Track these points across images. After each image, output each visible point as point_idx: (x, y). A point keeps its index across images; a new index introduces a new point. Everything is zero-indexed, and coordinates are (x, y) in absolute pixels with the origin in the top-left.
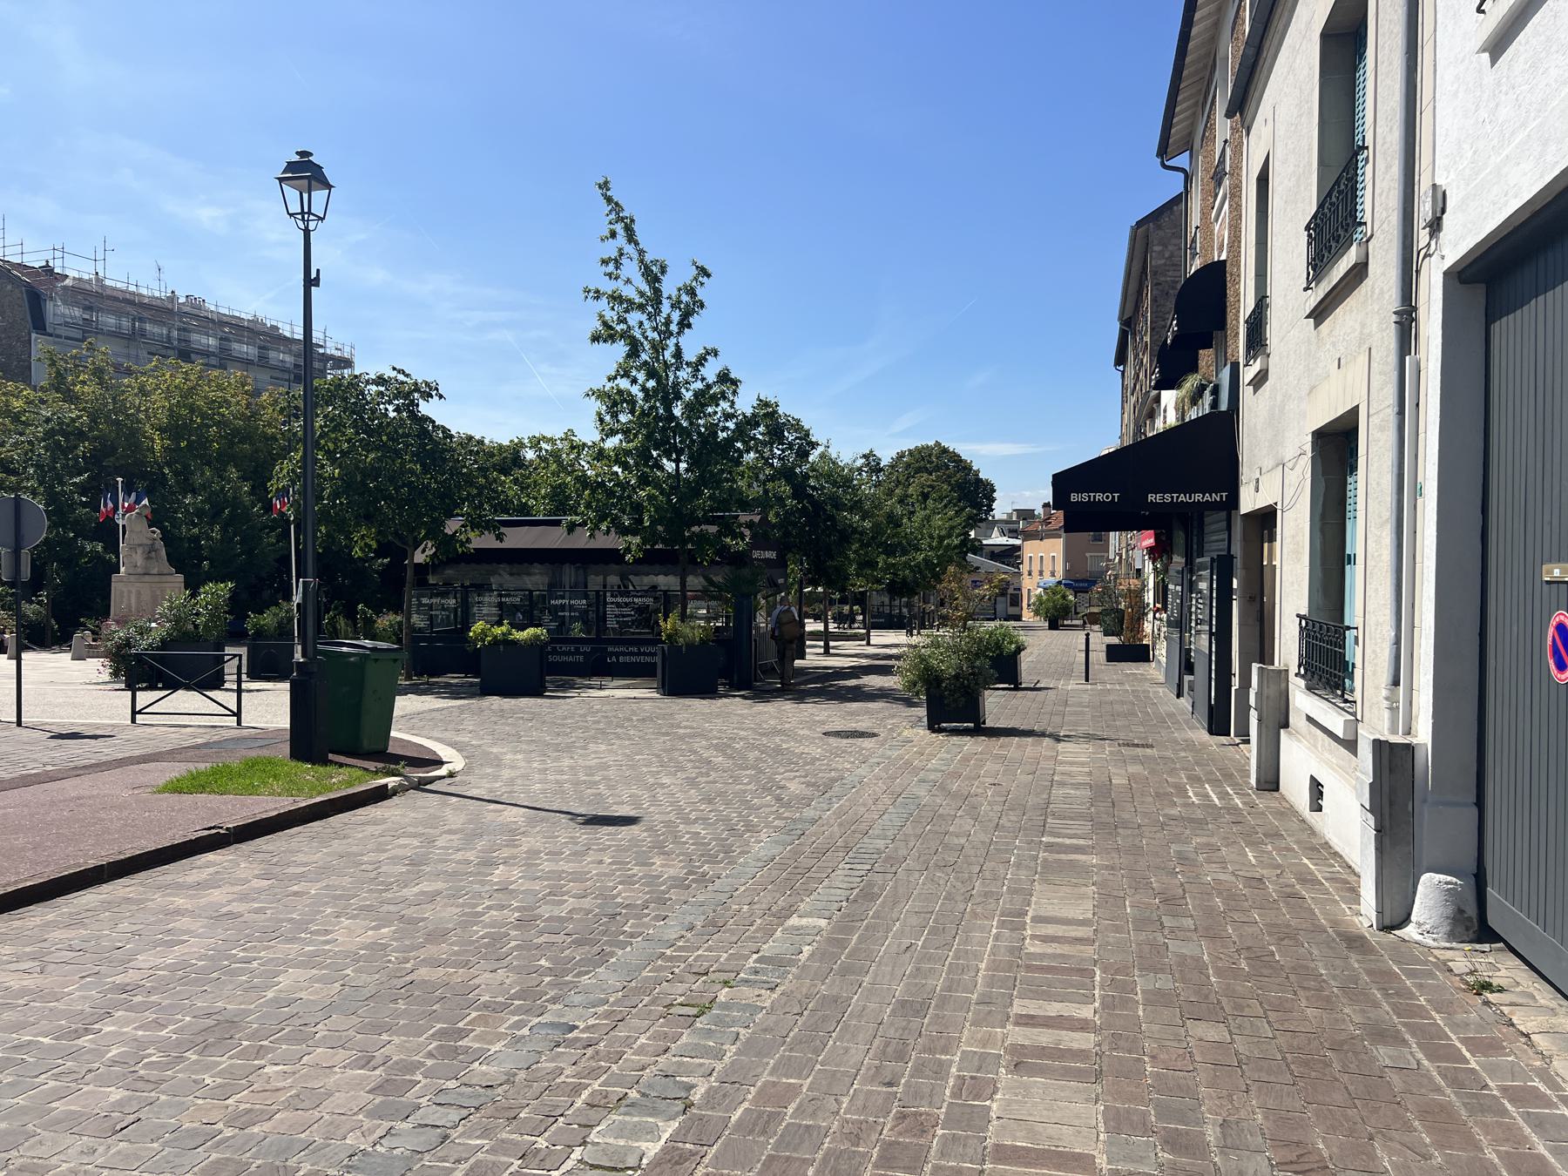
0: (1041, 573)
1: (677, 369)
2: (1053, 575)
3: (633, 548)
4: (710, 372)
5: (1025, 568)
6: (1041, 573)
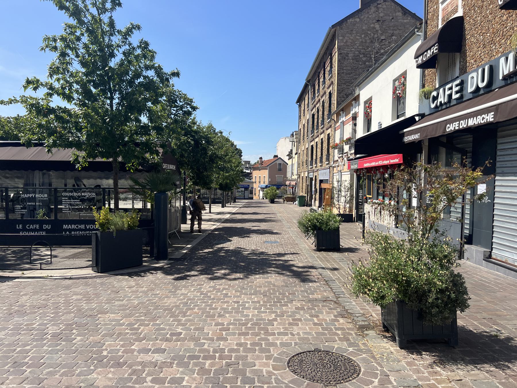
0: (260, 182)
1: (112, 35)
2: (264, 183)
3: (80, 160)
4: (135, 39)
5: (253, 180)
6: (260, 182)
